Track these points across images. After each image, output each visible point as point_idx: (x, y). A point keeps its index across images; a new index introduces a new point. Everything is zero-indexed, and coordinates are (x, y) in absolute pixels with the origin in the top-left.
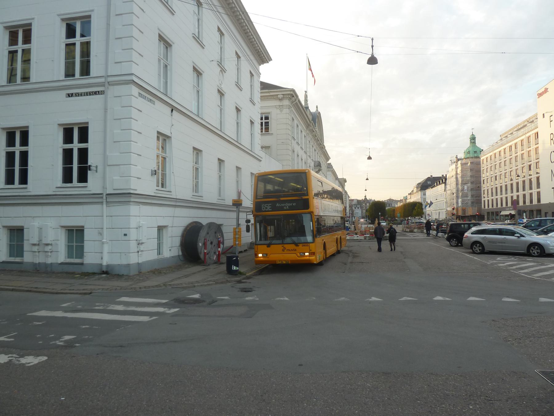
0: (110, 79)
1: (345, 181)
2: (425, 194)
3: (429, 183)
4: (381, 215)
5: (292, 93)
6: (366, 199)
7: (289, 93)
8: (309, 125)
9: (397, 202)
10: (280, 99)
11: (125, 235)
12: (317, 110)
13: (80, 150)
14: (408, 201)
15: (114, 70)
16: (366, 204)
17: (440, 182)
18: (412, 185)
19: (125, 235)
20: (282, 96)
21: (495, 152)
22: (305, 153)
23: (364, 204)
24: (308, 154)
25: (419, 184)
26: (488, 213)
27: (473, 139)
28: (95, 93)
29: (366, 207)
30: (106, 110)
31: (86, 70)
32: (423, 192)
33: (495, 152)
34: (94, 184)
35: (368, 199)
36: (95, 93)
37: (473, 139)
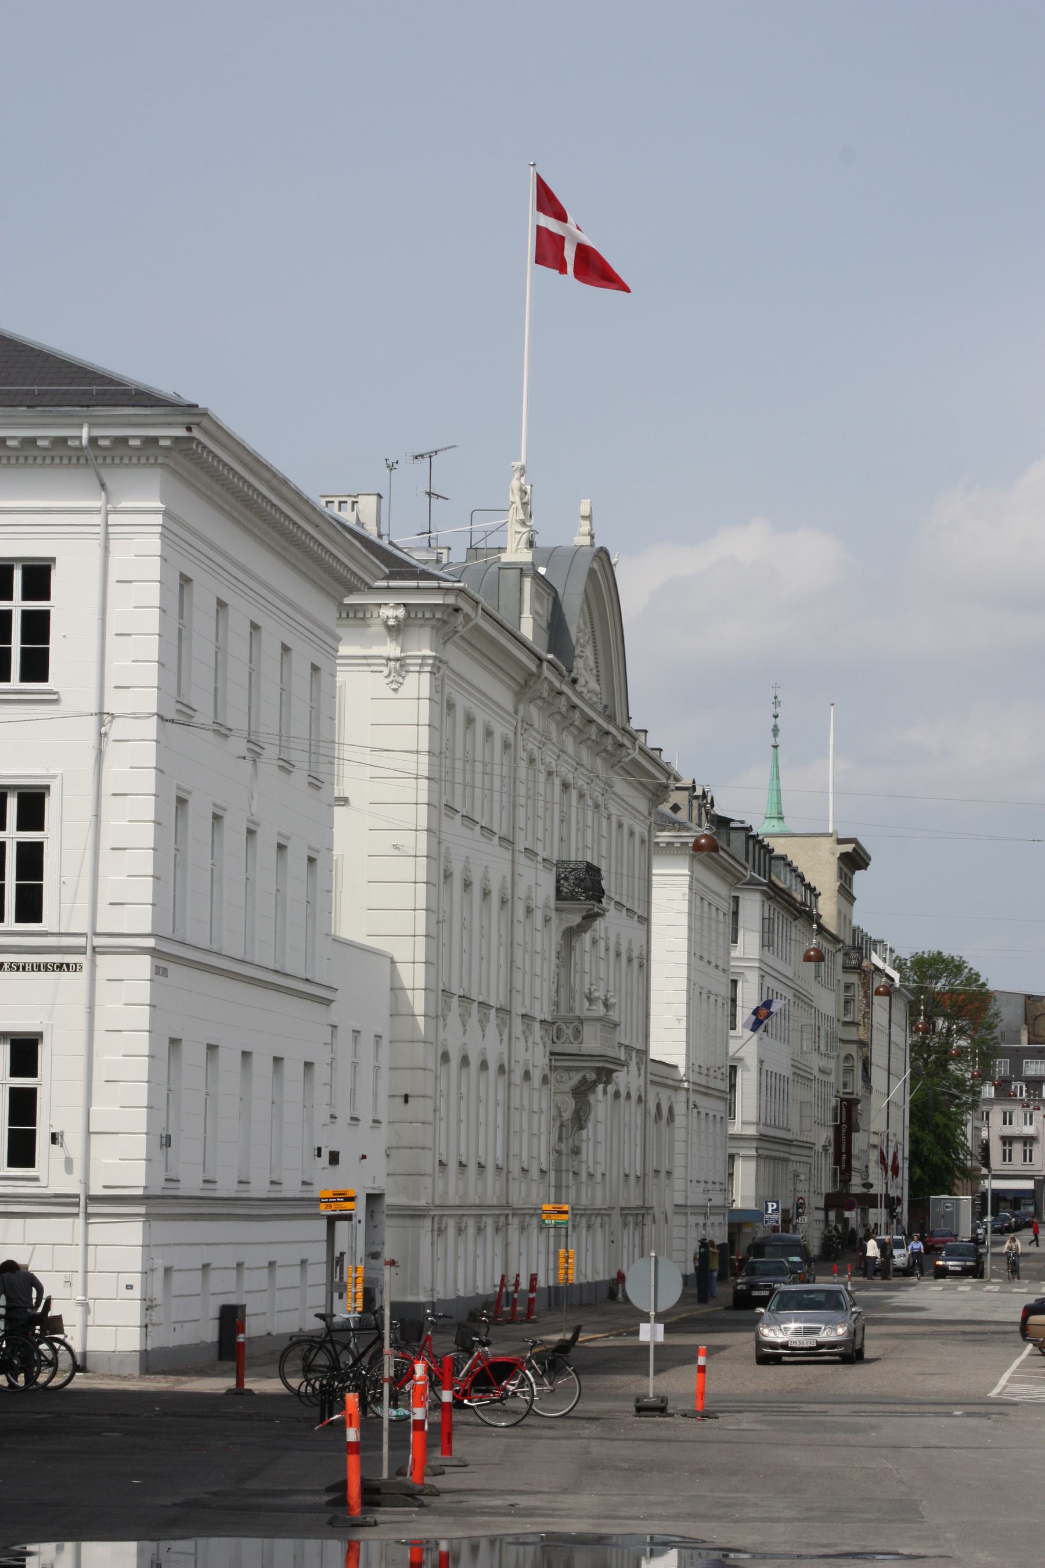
22: (507, 842)
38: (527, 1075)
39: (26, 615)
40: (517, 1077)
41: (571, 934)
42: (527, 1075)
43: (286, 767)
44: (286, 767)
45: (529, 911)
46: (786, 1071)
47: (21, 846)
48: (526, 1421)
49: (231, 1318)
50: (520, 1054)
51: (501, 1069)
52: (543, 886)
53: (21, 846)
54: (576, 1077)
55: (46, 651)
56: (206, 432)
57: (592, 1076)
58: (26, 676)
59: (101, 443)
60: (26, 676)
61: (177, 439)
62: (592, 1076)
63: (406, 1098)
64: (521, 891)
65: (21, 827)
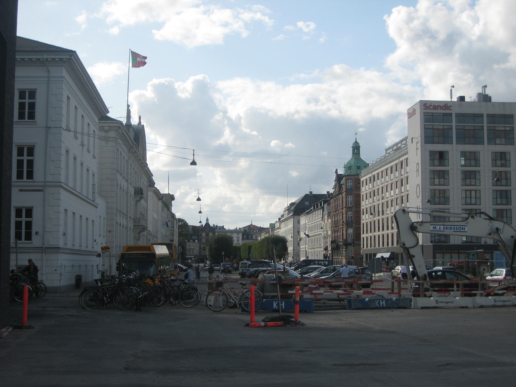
0: (48, 184)
1: (172, 198)
2: (299, 222)
3: (307, 203)
4: (226, 256)
5: (119, 125)
6: (207, 224)
7: (116, 125)
8: (131, 147)
9: (261, 230)
10: (106, 131)
11: (56, 270)
12: (140, 122)
13: (27, 222)
14: (276, 233)
15: (49, 178)
16: (207, 235)
17: (317, 207)
18: (280, 205)
19: (56, 270)
20: (108, 128)
21: (401, 159)
22: (127, 181)
23: (204, 234)
24: (129, 182)
25: (292, 204)
26: (367, 255)
27: (356, 148)
28: (38, 190)
29: (207, 240)
30: (44, 201)
31: (30, 175)
32: (296, 218)
33: (401, 159)
34: (36, 241)
35: (211, 225)
36: (38, 190)
37: (356, 148)
38: (130, 229)
39: (29, 103)
40: (129, 229)
41: (137, 201)
42: (130, 229)
43: (89, 151)
44: (89, 151)
45: (130, 196)
46: (164, 234)
47: (28, 160)
48: (224, 310)
49: (79, 278)
50: (129, 225)
51: (126, 227)
52: (132, 191)
53: (28, 160)
54: (139, 230)
55: (32, 171)
56: (74, 57)
57: (142, 230)
58: (28, 178)
59: (49, 60)
60: (28, 178)
61: (68, 59)
62: (142, 230)
63: (110, 232)
64: (129, 192)
65: (28, 156)
